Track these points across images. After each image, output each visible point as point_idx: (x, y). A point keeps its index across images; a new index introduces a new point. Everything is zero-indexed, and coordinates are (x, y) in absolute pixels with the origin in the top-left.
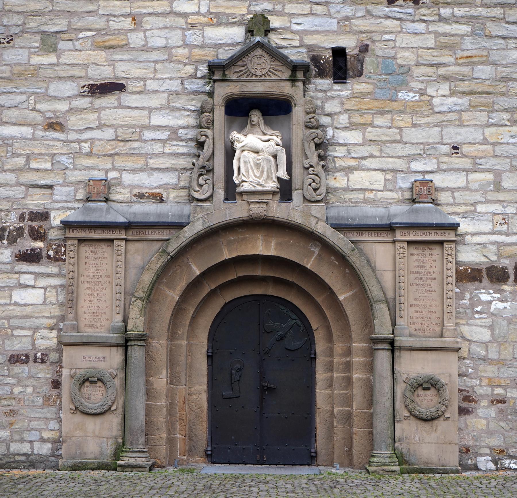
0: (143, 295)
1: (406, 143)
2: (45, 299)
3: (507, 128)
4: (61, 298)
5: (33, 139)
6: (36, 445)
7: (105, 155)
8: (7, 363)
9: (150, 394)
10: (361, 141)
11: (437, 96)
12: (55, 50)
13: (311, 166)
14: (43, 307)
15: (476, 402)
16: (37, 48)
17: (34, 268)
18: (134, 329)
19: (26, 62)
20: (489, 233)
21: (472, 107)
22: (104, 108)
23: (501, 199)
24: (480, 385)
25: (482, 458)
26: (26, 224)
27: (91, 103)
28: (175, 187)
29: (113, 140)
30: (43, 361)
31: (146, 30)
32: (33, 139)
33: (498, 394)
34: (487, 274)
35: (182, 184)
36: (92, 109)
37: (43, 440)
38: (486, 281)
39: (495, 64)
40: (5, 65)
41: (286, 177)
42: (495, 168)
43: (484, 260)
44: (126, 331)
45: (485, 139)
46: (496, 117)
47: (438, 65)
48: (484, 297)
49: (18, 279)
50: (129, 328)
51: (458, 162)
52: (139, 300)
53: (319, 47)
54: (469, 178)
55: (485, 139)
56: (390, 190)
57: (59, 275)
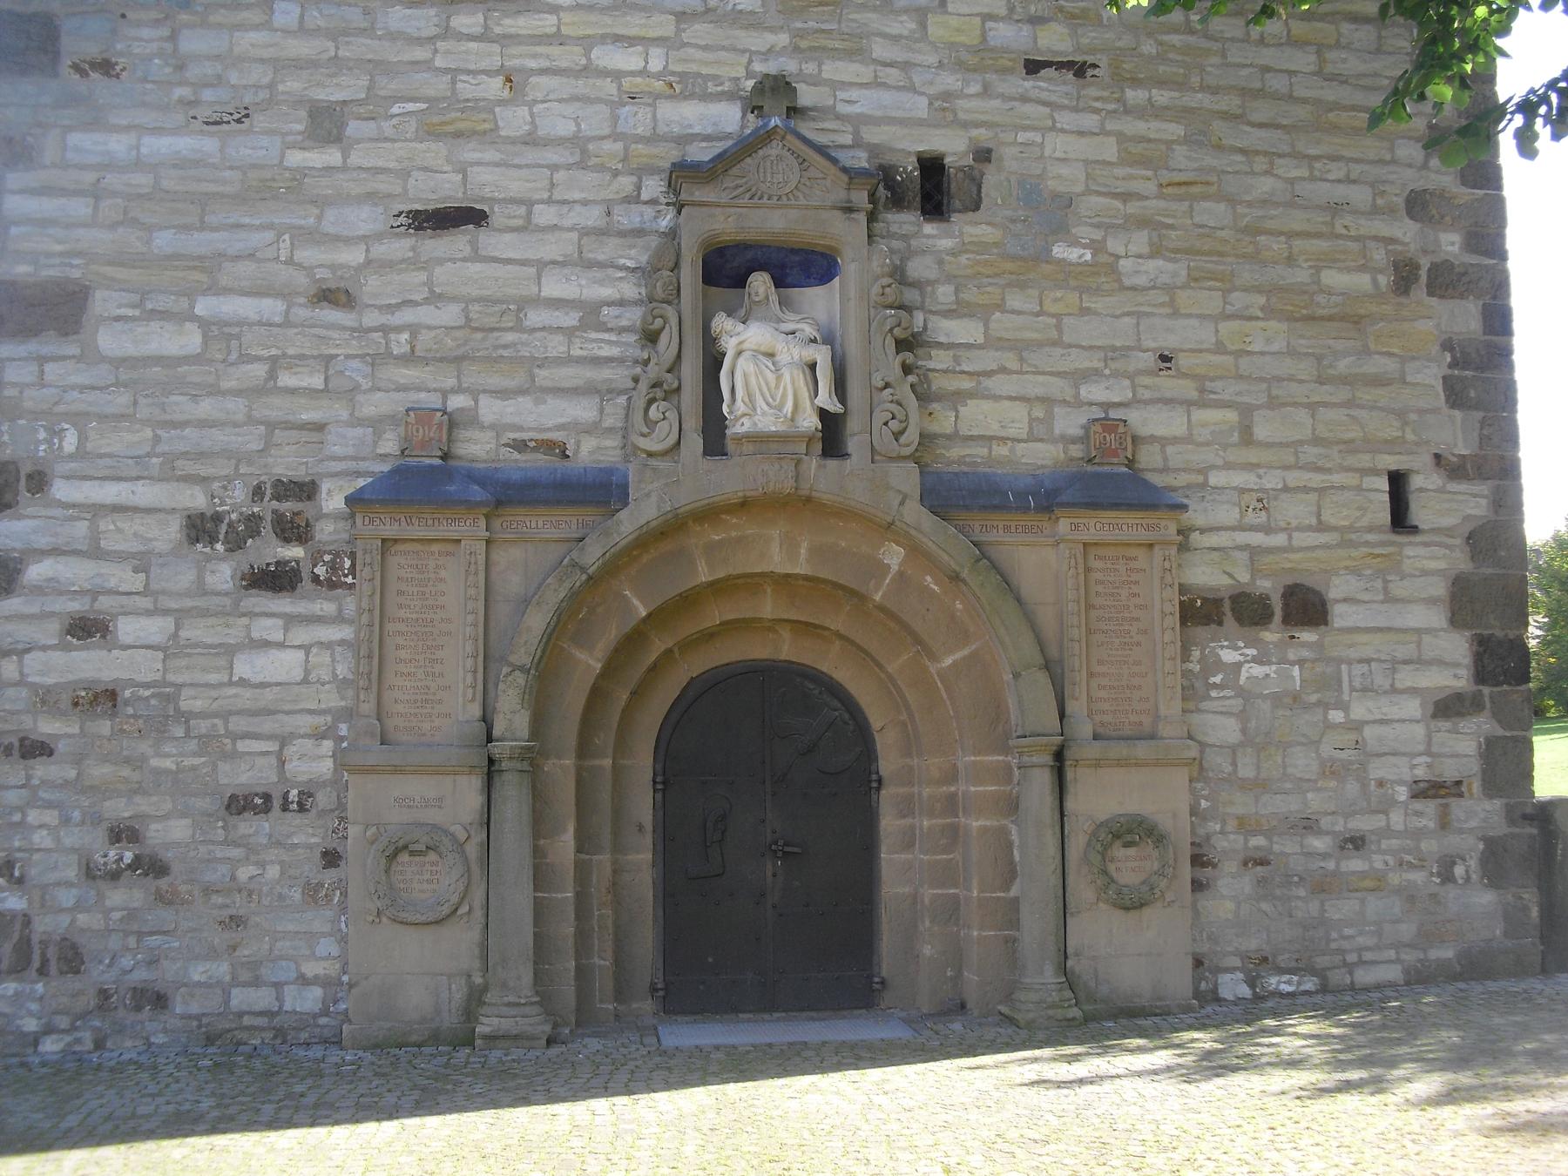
0: (527, 661)
1: (1070, 346)
2: (307, 672)
3: (1261, 324)
4: (342, 670)
5: (287, 323)
6: (290, 992)
7: (441, 360)
8: (223, 812)
9: (541, 876)
10: (981, 340)
11: (1127, 256)
12: (338, 140)
13: (887, 386)
14: (303, 689)
15: (1214, 866)
16: (300, 133)
17: (283, 604)
18: (508, 735)
19: (276, 162)
20: (1233, 529)
21: (1194, 279)
22: (441, 261)
23: (1254, 461)
24: (1222, 832)
25: (1228, 976)
26: (265, 508)
27: (413, 249)
28: (592, 429)
29: (460, 327)
30: (302, 808)
31: (535, 102)
32: (287, 323)
33: (1257, 848)
34: (1233, 610)
35: (608, 422)
36: (414, 263)
37: (304, 981)
38: (1229, 620)
39: (1232, 201)
40: (231, 168)
41: (834, 407)
42: (1239, 399)
43: (1227, 581)
44: (490, 739)
45: (1219, 343)
46: (1238, 300)
47: (1126, 197)
48: (1228, 656)
49: (248, 627)
50: (496, 732)
51: (1169, 385)
52: (517, 673)
53: (892, 150)
54: (1193, 418)
55: (1219, 343)
56: (1041, 440)
57: (339, 619)
